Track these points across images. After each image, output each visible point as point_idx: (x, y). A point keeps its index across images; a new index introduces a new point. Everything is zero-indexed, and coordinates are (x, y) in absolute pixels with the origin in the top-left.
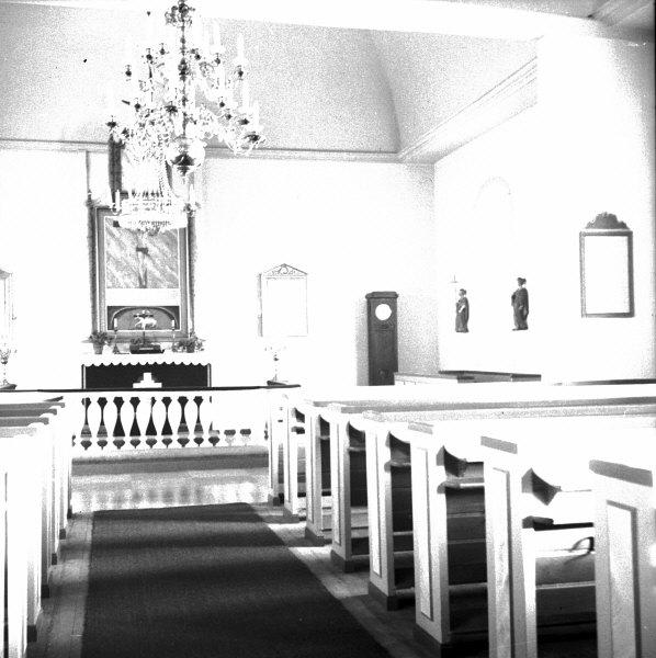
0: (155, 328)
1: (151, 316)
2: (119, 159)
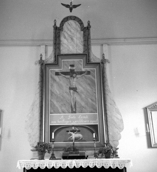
0: (82, 140)
1: (79, 131)
2: (59, 36)
